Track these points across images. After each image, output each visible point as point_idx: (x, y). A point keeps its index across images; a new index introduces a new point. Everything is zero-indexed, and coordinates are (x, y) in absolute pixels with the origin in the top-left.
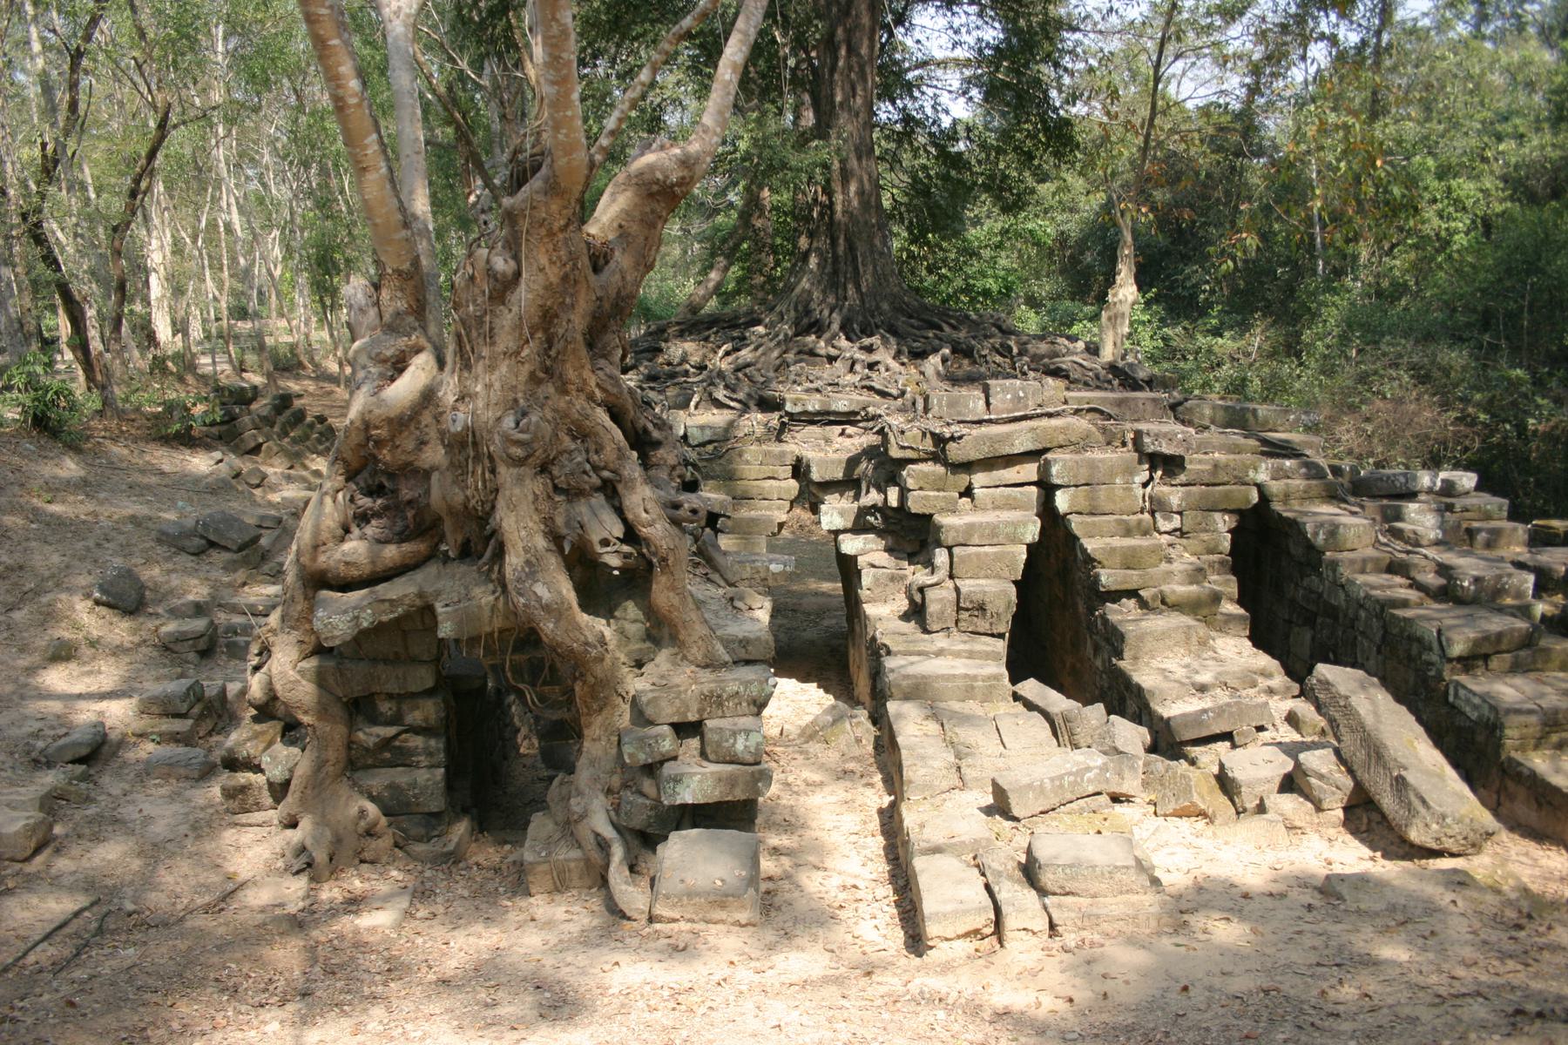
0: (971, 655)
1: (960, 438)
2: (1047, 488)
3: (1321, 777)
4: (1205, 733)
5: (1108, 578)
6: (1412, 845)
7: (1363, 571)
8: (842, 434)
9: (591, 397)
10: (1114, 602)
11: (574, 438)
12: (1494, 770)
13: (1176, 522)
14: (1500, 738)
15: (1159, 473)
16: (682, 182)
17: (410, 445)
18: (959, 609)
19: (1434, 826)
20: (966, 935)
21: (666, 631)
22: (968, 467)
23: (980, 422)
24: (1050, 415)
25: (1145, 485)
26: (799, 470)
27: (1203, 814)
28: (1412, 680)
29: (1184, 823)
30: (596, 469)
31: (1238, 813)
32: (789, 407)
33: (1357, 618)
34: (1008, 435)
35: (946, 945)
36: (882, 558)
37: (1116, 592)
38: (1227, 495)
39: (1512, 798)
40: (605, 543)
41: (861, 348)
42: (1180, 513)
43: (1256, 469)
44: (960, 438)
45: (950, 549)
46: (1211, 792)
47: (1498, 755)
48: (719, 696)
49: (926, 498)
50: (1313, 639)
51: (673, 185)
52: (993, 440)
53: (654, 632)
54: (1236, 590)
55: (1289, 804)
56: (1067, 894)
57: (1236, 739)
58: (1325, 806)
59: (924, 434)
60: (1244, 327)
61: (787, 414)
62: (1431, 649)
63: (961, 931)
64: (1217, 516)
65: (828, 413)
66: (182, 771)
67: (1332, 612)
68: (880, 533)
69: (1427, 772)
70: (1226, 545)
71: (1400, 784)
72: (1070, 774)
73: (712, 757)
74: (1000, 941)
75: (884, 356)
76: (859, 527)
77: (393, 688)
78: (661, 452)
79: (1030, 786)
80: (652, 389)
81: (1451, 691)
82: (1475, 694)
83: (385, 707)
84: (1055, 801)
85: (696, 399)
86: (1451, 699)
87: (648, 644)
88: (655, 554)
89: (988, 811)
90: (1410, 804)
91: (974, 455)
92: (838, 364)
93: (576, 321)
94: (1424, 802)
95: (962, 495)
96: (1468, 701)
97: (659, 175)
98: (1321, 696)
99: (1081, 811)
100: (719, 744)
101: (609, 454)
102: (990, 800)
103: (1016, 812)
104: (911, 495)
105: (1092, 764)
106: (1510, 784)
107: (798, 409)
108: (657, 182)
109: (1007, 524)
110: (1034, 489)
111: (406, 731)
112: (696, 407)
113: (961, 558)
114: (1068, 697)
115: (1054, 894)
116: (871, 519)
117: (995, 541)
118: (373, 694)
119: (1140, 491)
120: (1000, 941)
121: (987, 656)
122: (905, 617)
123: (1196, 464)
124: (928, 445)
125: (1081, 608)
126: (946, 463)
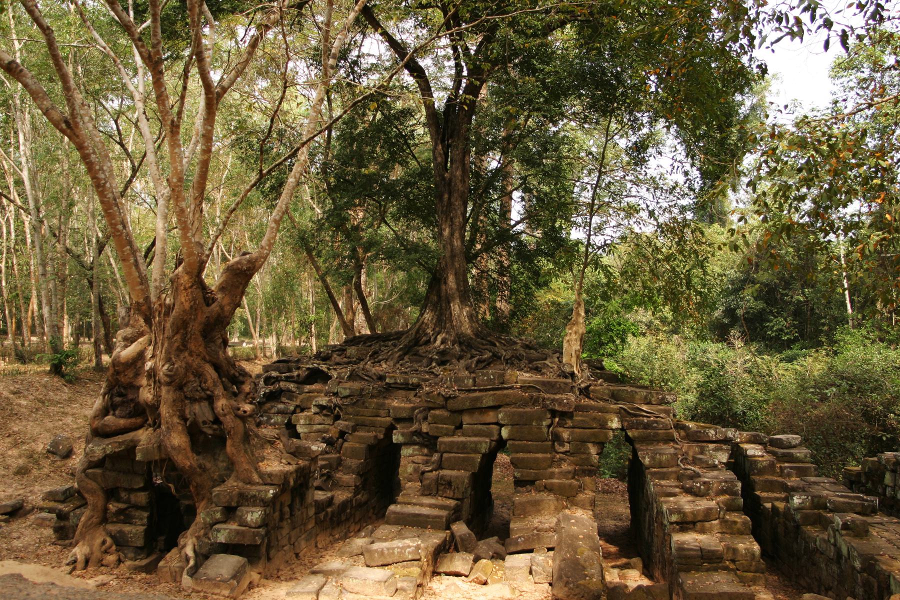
9: (204, 359)
11: (195, 376)
15: (557, 419)
17: (131, 375)
25: (549, 426)
30: (203, 389)
38: (594, 435)
40: (204, 423)
42: (569, 443)
44: (455, 397)
49: (437, 428)
52: (477, 399)
66: (48, 523)
77: (125, 485)
83: (123, 495)
91: (461, 407)
93: (195, 327)
101: (210, 382)
108: (239, 269)
111: (132, 507)
118: (117, 488)
121: (519, 530)
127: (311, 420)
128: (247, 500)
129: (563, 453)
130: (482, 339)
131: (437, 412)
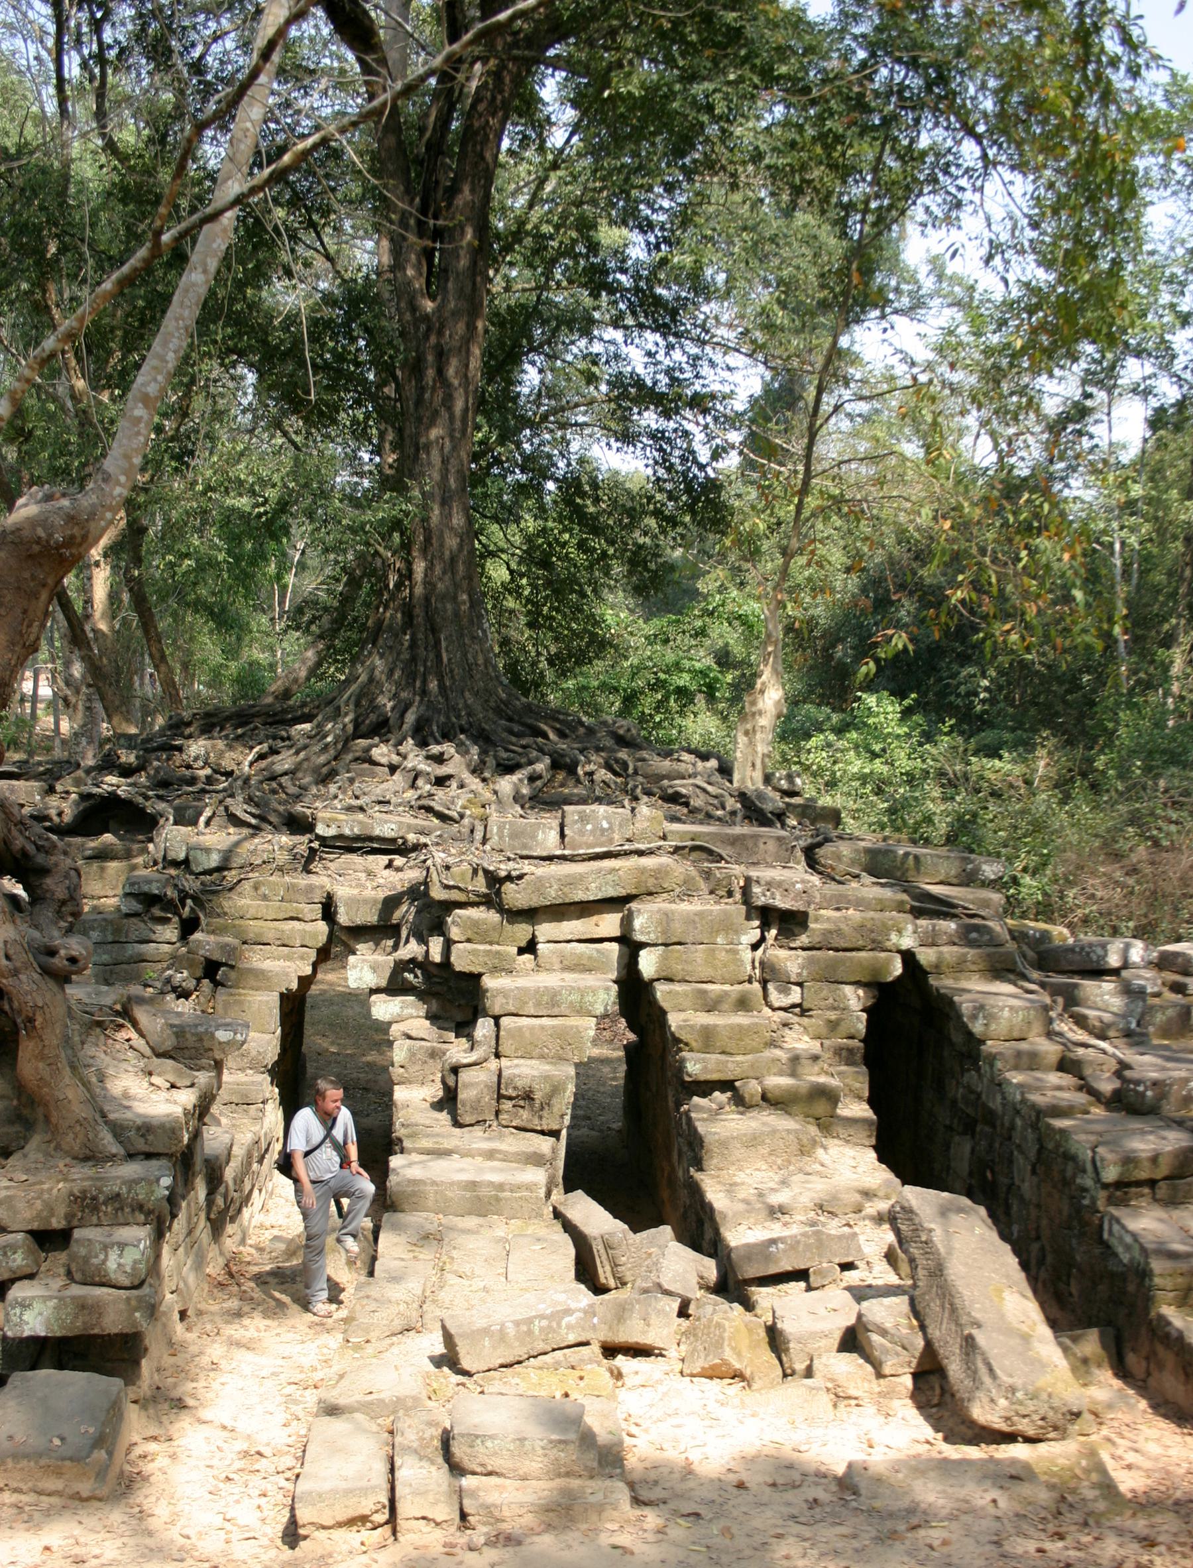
0: (490, 1155)
1: (520, 877)
2: (630, 946)
3: (884, 1333)
4: (773, 1270)
5: (695, 1066)
6: (972, 1423)
7: (1016, 1068)
8: (389, 866)
10: (704, 1095)
12: (1143, 1330)
13: (795, 995)
14: (1149, 1289)
15: (774, 932)
16: (70, 542)
18: (500, 1097)
19: (1003, 1402)
20: (351, 1522)
21: (40, 1111)
22: (530, 915)
23: (550, 858)
24: (641, 853)
25: (755, 947)
26: (328, 910)
27: (737, 1375)
28: (1066, 1212)
29: (714, 1387)
31: (785, 1375)
32: (320, 829)
33: (1012, 1127)
34: (582, 877)
35: (321, 1535)
36: (421, 1026)
37: (707, 1082)
39: (1161, 1366)
41: (428, 757)
42: (800, 984)
43: (900, 931)
44: (520, 877)
45: (497, 1019)
46: (754, 1346)
47: (1147, 1310)
48: (94, 1198)
50: (973, 1151)
51: (59, 546)
52: (572, 882)
53: (26, 1112)
54: (866, 1087)
55: (848, 1366)
56: (490, 1474)
57: (812, 1279)
58: (887, 1370)
59: (475, 872)
60: (1025, 746)
61: (318, 837)
62: (1084, 1171)
63: (341, 1517)
64: (848, 990)
65: (371, 839)
67: (990, 1117)
68: (422, 995)
69: (1009, 1331)
70: (862, 1027)
71: (969, 1343)
72: (542, 1317)
73: (78, 1276)
74: (394, 1532)
75: (456, 765)
76: (395, 987)
78: (49, 881)
79: (486, 1331)
80: (160, 797)
81: (1106, 1226)
82: (1127, 1231)
84: (520, 1352)
85: (207, 813)
86: (1106, 1236)
87: (17, 1128)
88: (20, 1012)
89: (438, 1362)
90: (975, 1372)
91: (535, 901)
92: (397, 776)
94: (991, 1370)
95: (521, 951)
96: (1121, 1239)
97: (40, 532)
98: (903, 1227)
99: (556, 1366)
100: (86, 1260)
102: (440, 1349)
103: (466, 1364)
104: (456, 948)
105: (573, 1305)
106: (1160, 1349)
107: (331, 832)
108: (38, 541)
109: (571, 990)
110: (615, 946)
112: (208, 824)
113: (509, 1031)
114: (615, 1217)
115: (474, 1473)
116: (409, 976)
117: (556, 1011)
119: (747, 955)
120: (394, 1532)
121: (536, 1160)
122: (438, 1106)
123: (823, 920)
124: (480, 885)
125: (671, 1104)
126: (501, 910)
127: (117, 930)
128: (95, 1209)
129: (785, 1009)
130: (510, 720)
131: (472, 913)
